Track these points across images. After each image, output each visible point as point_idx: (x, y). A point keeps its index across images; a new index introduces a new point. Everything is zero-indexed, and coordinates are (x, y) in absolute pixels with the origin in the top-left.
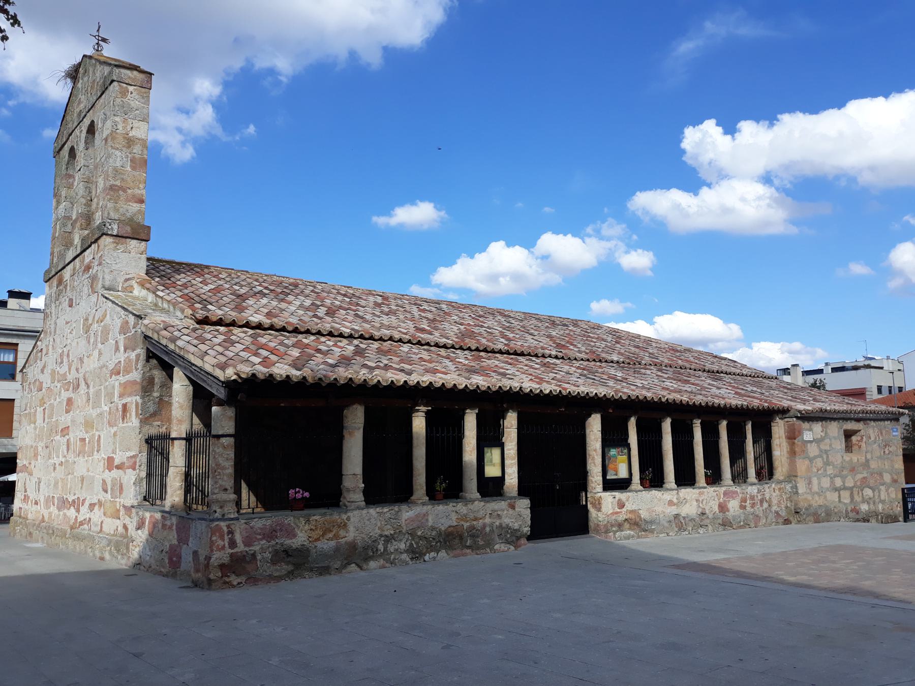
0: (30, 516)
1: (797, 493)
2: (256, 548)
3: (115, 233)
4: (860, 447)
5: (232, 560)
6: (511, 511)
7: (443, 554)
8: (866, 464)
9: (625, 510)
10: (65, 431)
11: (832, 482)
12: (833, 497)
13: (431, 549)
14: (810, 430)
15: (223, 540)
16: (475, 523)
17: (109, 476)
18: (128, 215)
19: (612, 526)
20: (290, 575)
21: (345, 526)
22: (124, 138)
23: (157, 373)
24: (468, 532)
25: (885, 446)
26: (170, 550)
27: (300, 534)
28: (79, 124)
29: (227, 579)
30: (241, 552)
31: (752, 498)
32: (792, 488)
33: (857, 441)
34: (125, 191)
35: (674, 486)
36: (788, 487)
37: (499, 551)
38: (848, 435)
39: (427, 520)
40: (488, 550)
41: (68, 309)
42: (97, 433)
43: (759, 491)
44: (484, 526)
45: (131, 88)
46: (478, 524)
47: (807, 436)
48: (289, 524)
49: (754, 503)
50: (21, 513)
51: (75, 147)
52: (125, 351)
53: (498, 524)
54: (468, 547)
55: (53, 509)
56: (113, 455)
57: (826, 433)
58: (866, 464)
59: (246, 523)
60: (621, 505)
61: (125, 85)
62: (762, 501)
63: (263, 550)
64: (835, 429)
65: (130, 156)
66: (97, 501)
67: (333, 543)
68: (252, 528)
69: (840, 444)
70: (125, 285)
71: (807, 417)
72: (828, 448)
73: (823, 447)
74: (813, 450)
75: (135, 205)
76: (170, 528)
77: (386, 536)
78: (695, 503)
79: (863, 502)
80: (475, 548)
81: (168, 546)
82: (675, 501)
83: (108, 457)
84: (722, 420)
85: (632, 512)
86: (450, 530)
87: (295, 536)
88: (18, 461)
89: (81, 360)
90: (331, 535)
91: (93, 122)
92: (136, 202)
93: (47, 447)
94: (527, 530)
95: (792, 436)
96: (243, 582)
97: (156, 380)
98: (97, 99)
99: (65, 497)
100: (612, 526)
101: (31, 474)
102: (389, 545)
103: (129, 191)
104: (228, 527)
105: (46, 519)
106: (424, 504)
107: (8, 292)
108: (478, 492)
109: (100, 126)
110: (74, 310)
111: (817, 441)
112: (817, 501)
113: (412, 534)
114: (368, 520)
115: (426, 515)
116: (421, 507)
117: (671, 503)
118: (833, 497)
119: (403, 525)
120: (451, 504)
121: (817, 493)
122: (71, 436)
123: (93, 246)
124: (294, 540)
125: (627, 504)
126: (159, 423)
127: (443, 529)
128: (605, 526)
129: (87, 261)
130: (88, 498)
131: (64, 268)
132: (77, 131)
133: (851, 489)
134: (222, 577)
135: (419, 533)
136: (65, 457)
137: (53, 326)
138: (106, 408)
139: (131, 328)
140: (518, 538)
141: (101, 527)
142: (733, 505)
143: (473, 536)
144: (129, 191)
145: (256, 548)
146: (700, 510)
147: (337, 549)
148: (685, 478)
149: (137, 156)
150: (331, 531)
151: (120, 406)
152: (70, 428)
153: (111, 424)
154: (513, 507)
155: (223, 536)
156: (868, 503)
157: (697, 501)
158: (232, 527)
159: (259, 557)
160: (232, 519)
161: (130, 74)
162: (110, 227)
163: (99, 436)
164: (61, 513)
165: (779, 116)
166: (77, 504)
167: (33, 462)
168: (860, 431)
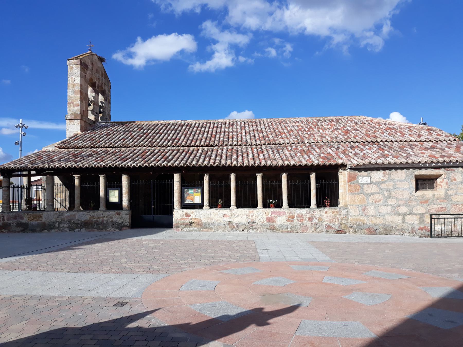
2: (11, 222)
4: (442, 186)
5: (3, 225)
7: (83, 230)
9: (191, 218)
16: (98, 219)
18: (74, 111)
19: (181, 224)
21: (41, 217)
27: (25, 218)
33: (440, 182)
34: (73, 103)
37: (109, 231)
39: (75, 217)
40: (105, 230)
44: (103, 221)
45: (74, 66)
49: (302, 219)
54: (95, 228)
63: (13, 222)
67: (36, 222)
71: (358, 168)
80: (98, 229)
84: (282, 173)
86: (86, 221)
96: (7, 232)
100: (181, 224)
103: (74, 103)
104: (2, 215)
113: (70, 221)
120: (87, 212)
124: (23, 220)
125: (192, 215)
128: (177, 224)
135: (72, 221)
143: (97, 224)
144: (74, 103)
147: (38, 224)
150: (36, 218)
158: (3, 215)
159: (12, 224)
165: (126, 48)
168: (442, 175)
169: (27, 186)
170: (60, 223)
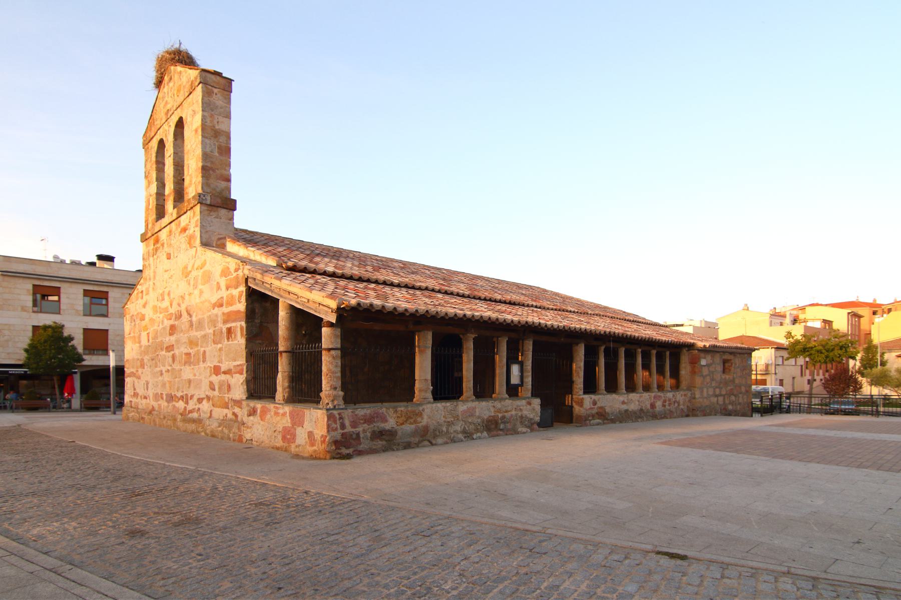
0: (140, 407)
1: (694, 398)
2: (360, 429)
3: (208, 202)
6: (529, 407)
8: (733, 381)
10: (170, 348)
11: (714, 392)
12: (714, 400)
13: (477, 430)
14: (705, 358)
15: (336, 424)
16: (506, 414)
17: (215, 379)
18: (218, 190)
20: (385, 450)
22: (212, 129)
23: (257, 305)
24: (501, 420)
25: (743, 370)
26: (283, 430)
27: (391, 420)
28: (167, 121)
29: (339, 451)
30: (350, 432)
31: (670, 400)
32: (691, 394)
34: (214, 171)
35: (624, 391)
36: (689, 394)
38: (725, 362)
39: (475, 412)
41: (166, 261)
42: (202, 349)
43: (674, 396)
45: (216, 91)
46: (507, 415)
47: (703, 362)
48: (383, 413)
50: (131, 404)
51: (164, 139)
52: (227, 289)
53: (520, 414)
54: (501, 430)
55: (164, 404)
56: (220, 364)
57: (713, 361)
58: (733, 381)
59: (352, 412)
60: (595, 403)
61: (210, 87)
62: (674, 402)
63: (365, 431)
64: (718, 359)
65: (217, 144)
66: (205, 396)
67: (413, 426)
68: (356, 415)
69: (720, 368)
70: (219, 243)
72: (713, 370)
73: (711, 369)
74: (705, 371)
75: (223, 183)
76: (284, 414)
77: (449, 422)
78: (637, 403)
79: (730, 404)
81: (281, 428)
82: (626, 401)
83: (214, 366)
85: (601, 408)
87: (386, 421)
88: (125, 369)
89: (183, 298)
90: (412, 421)
91: (181, 119)
92: (223, 180)
93: (153, 360)
94: (538, 419)
95: (694, 362)
97: (257, 311)
98: (185, 99)
99: (173, 393)
101: (139, 378)
102: (450, 428)
104: (339, 414)
105: (157, 409)
106: (473, 401)
107: (97, 256)
108: (507, 393)
109: (189, 119)
110: (173, 261)
111: (708, 365)
112: (706, 402)
114: (437, 411)
115: (474, 408)
116: (471, 402)
117: (623, 403)
118: (714, 400)
119: (460, 415)
121: (706, 398)
122: (177, 352)
123: (189, 212)
124: (386, 424)
126: (260, 341)
127: (485, 418)
129: (183, 224)
130: (197, 394)
131: (160, 230)
132: (165, 127)
133: (724, 396)
134: (336, 450)
136: (171, 366)
137: (152, 275)
138: (211, 331)
139: (233, 272)
140: (532, 424)
141: (211, 414)
142: (659, 404)
145: (360, 429)
146: (640, 407)
148: (612, 387)
149: (223, 145)
150: (412, 418)
151: (224, 330)
152: (175, 346)
153: (215, 342)
154: (529, 404)
155: (336, 421)
156: (732, 405)
157: (639, 401)
159: (362, 435)
160: (342, 409)
161: (214, 79)
162: (204, 198)
163: (204, 352)
164: (171, 404)
166: (186, 399)
167: (140, 370)
169: (521, 341)
170: (450, 424)
